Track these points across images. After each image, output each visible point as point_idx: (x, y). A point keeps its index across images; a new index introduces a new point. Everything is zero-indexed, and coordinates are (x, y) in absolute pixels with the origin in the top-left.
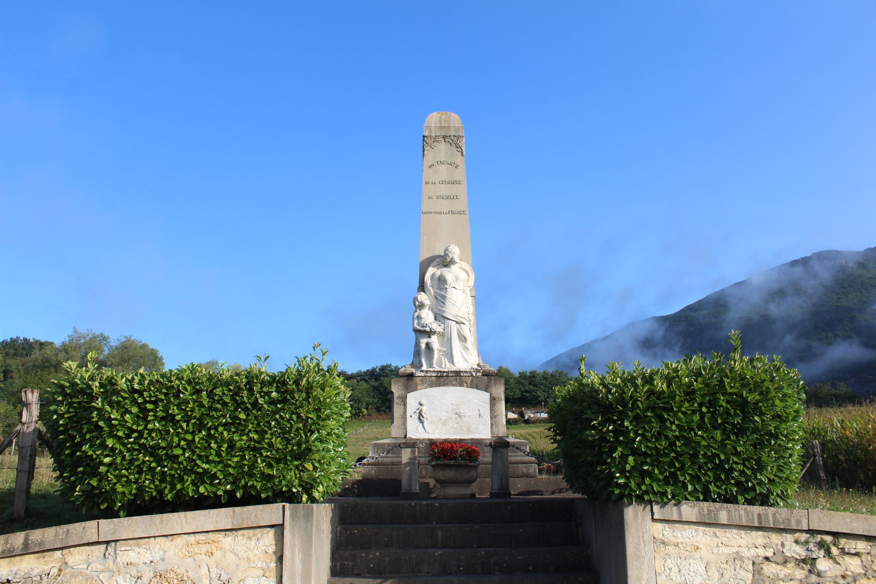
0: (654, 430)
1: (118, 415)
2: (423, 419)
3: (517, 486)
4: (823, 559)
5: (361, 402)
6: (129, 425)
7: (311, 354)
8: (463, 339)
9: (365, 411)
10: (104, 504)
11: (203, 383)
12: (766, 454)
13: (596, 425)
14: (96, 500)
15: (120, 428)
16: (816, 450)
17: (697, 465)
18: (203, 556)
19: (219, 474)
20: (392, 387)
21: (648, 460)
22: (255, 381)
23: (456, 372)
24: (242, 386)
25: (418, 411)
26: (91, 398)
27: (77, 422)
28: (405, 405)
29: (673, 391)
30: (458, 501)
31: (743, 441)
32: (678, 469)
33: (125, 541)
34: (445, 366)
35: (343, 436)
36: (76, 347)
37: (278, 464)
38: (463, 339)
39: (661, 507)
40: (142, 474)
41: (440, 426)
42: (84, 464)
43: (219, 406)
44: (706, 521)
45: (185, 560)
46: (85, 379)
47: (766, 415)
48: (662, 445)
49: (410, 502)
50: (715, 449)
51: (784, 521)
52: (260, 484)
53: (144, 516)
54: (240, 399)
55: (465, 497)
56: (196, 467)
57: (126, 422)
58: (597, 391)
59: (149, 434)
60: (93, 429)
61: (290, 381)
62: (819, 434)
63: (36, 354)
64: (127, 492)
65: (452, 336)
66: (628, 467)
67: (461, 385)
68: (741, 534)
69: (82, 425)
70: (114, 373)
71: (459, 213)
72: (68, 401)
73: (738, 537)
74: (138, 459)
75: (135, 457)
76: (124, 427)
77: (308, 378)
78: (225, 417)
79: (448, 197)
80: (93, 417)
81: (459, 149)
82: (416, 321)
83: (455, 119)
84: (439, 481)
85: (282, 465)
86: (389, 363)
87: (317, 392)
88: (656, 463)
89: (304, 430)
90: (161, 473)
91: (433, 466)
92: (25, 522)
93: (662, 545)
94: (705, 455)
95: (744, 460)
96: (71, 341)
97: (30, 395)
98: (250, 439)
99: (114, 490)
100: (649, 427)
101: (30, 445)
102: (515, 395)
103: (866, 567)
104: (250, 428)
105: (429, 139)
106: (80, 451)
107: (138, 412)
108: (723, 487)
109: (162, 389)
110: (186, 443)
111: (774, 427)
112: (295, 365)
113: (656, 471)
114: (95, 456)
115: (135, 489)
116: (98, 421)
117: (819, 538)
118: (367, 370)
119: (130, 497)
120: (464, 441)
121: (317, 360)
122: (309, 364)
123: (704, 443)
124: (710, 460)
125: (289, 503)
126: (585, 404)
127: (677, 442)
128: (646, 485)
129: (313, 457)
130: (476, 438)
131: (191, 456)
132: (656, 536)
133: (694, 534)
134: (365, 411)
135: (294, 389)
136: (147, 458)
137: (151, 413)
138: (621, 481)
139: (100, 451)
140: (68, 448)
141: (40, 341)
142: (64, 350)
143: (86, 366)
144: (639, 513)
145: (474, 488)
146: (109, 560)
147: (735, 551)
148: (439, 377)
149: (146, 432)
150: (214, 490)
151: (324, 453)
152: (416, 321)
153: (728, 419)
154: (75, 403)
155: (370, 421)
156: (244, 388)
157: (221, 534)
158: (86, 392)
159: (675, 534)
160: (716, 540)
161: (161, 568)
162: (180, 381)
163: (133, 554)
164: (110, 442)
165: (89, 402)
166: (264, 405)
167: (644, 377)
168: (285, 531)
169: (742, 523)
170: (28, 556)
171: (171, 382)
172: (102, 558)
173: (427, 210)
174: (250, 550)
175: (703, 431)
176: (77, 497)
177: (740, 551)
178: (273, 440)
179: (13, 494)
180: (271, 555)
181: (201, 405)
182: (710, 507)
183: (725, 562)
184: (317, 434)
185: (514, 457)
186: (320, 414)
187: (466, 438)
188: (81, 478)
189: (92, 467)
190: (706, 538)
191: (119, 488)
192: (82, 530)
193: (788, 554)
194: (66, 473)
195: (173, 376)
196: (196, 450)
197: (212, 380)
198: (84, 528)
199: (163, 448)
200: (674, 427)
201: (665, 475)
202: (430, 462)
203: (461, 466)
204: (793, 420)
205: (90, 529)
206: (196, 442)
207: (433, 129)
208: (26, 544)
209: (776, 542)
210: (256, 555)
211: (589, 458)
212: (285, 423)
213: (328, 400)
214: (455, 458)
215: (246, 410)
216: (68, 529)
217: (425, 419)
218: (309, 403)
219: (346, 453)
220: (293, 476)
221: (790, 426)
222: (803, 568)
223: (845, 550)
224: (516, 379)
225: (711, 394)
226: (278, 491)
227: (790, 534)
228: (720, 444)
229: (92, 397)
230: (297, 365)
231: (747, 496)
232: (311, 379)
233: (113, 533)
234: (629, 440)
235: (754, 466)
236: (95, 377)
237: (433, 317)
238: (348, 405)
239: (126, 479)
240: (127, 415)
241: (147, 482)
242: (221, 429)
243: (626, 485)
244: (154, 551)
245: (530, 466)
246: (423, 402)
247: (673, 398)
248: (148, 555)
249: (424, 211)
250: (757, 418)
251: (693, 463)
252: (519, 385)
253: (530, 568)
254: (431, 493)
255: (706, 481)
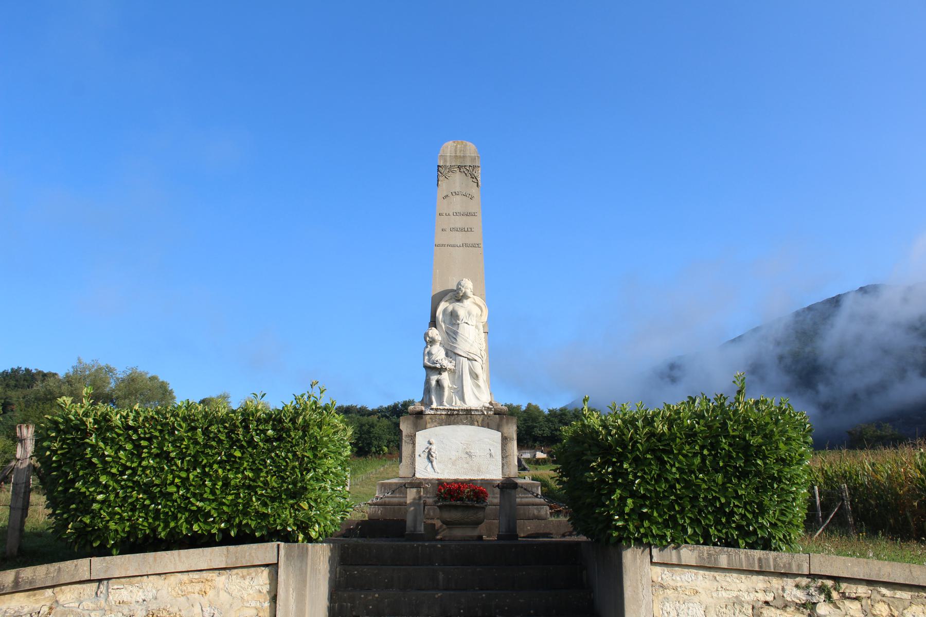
0: (653, 472)
1: (112, 452)
2: (432, 458)
3: (526, 528)
4: (823, 603)
5: (382, 439)
6: (123, 461)
7: (308, 392)
8: (475, 376)
9: (386, 449)
10: (97, 542)
11: (198, 420)
12: (768, 498)
13: (595, 466)
14: (89, 537)
15: (113, 465)
16: (844, 494)
17: (697, 509)
18: (197, 595)
19: (213, 512)
20: (401, 425)
21: (647, 503)
22: (251, 418)
23: (467, 410)
24: (238, 423)
25: (427, 450)
26: (84, 434)
27: (70, 459)
28: (414, 444)
29: (674, 433)
30: (462, 543)
31: (745, 485)
32: (678, 512)
33: (117, 580)
34: (456, 404)
35: (343, 475)
36: (80, 378)
37: (273, 502)
38: (475, 376)
39: (660, 551)
40: (136, 511)
41: (450, 466)
42: (77, 501)
43: (214, 444)
44: (706, 565)
45: (178, 598)
46: (79, 415)
47: (770, 459)
48: (662, 488)
49: (412, 543)
50: (715, 492)
51: (784, 565)
52: (255, 522)
53: (138, 554)
54: (236, 437)
55: (471, 538)
56: (190, 505)
57: (120, 459)
58: (598, 433)
59: (143, 471)
60: (87, 466)
61: (286, 419)
62: (851, 478)
63: (37, 385)
64: (120, 529)
65: (464, 373)
66: (627, 510)
67: (472, 424)
68: (741, 578)
69: (75, 461)
70: (109, 409)
71: (473, 246)
72: (61, 437)
73: (738, 581)
74: (131, 497)
75: (128, 494)
76: (117, 464)
77: (305, 416)
78: (220, 454)
79: (462, 230)
80: (87, 454)
81: (474, 180)
82: (426, 358)
83: (471, 149)
84: (445, 522)
85: (277, 504)
86: (411, 399)
87: (314, 430)
88: (655, 506)
89: (299, 468)
90: (155, 511)
91: (440, 507)
92: (18, 560)
93: (661, 589)
94: (705, 498)
95: (746, 503)
96: (76, 372)
97: (24, 430)
98: (246, 477)
99: (106, 527)
100: (649, 470)
101: (24, 481)
102: (543, 433)
103: (865, 611)
104: (245, 466)
105: (444, 168)
106: (73, 488)
107: (132, 449)
108: (724, 531)
109: (157, 425)
110: (180, 480)
111: (777, 470)
112: (292, 403)
113: (655, 514)
114: (88, 493)
115: (129, 527)
116: (91, 458)
117: (819, 582)
118: (388, 406)
119: (122, 534)
120: (473, 482)
121: (314, 397)
122: (306, 402)
123: (704, 486)
124: (711, 503)
125: (285, 542)
126: (586, 445)
127: (677, 485)
128: (645, 528)
129: (309, 496)
130: (486, 478)
131: (185, 494)
132: (655, 579)
133: (693, 578)
134: (386, 449)
135: (290, 427)
136: (141, 496)
137: (145, 450)
138: (620, 524)
139: (94, 488)
140: (61, 485)
141: (42, 372)
142: (68, 382)
143: (82, 402)
144: (638, 556)
145: (481, 530)
146: (101, 599)
147: (734, 596)
148: (449, 415)
149: (140, 469)
150: (208, 528)
151: (320, 492)
152: (426, 358)
153: (730, 462)
154: (68, 439)
155: (390, 459)
156: (240, 426)
157: (214, 573)
158: (80, 428)
159: (674, 578)
160: (716, 583)
161: (153, 606)
162: (175, 418)
163: (125, 592)
164: (103, 479)
165: (83, 439)
166: (260, 443)
167: (645, 419)
168: (279, 570)
169: (742, 566)
170: (18, 594)
171: (166, 418)
172: (93, 596)
173: (441, 242)
174: (244, 589)
175: (705, 474)
176: (71, 534)
177: (739, 596)
178: (269, 479)
179: (7, 532)
180: (265, 595)
181: (196, 443)
182: (709, 551)
183: (724, 606)
184: (313, 473)
185: (521, 498)
186: (316, 453)
187: (476, 479)
188: (73, 515)
189: (85, 504)
190: (705, 582)
191: (112, 525)
192: (74, 567)
193: (789, 599)
194: (58, 510)
195: (168, 412)
196: (191, 487)
197: (207, 417)
198: (76, 566)
199: (157, 486)
200: (674, 470)
201: (664, 518)
202: (436, 502)
203: (467, 507)
204: (797, 464)
205: (82, 567)
206: (191, 480)
207: (448, 159)
208: (16, 582)
209: (777, 586)
210: (250, 594)
211: (588, 500)
212: (281, 461)
213: (325, 439)
214: (462, 499)
215: (241, 447)
216: (59, 567)
217: (434, 459)
218: (305, 441)
219: (347, 493)
220: (287, 515)
221: (794, 470)
222: (803, 613)
223: (845, 595)
224: (545, 417)
225: (713, 436)
226: (273, 530)
227: (791, 578)
228: (721, 487)
229: (86, 434)
230: (294, 403)
231: (748, 540)
232: (307, 417)
233: (106, 571)
234: (629, 482)
235: (756, 509)
236: (90, 413)
237: (445, 353)
238: (347, 443)
239: (119, 516)
240: (122, 452)
241: (141, 520)
242: (215, 466)
243: (625, 528)
244: (147, 590)
245: (541, 508)
246: (432, 440)
247: (674, 440)
248: (140, 593)
249: (437, 243)
250: (759, 462)
251: (693, 506)
252: (549, 423)
253: (532, 612)
254: (437, 534)
255: (707, 525)
